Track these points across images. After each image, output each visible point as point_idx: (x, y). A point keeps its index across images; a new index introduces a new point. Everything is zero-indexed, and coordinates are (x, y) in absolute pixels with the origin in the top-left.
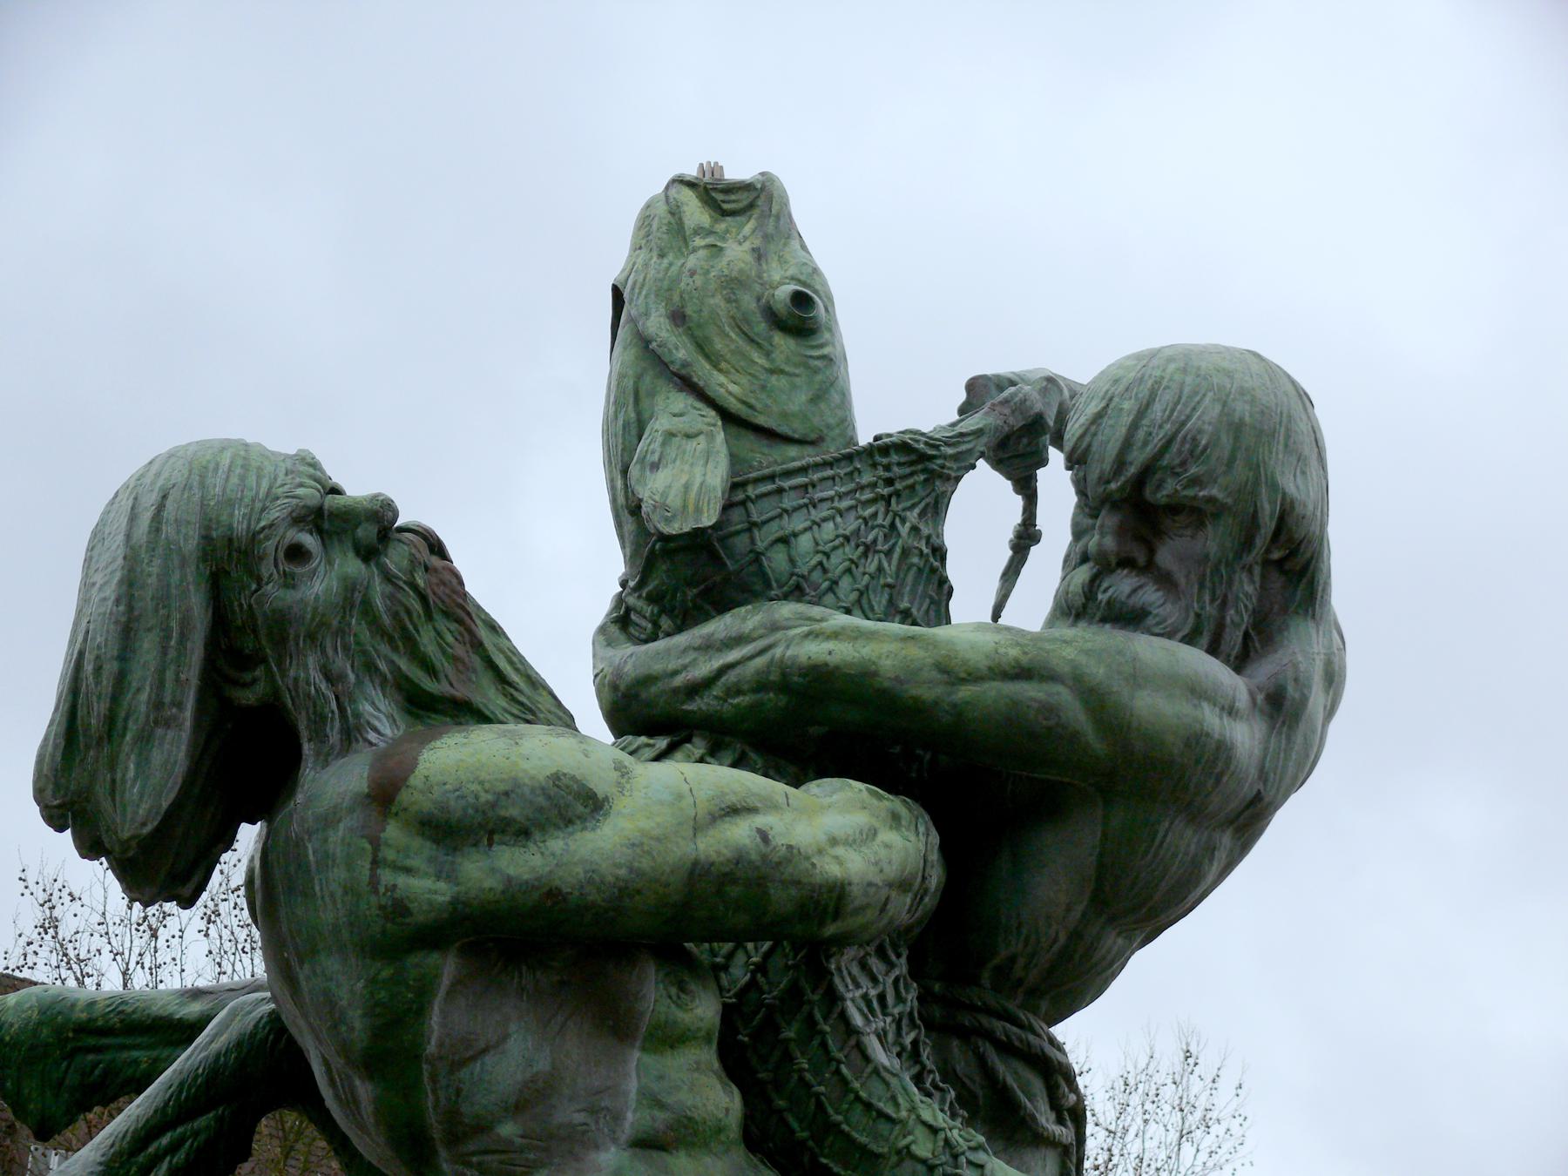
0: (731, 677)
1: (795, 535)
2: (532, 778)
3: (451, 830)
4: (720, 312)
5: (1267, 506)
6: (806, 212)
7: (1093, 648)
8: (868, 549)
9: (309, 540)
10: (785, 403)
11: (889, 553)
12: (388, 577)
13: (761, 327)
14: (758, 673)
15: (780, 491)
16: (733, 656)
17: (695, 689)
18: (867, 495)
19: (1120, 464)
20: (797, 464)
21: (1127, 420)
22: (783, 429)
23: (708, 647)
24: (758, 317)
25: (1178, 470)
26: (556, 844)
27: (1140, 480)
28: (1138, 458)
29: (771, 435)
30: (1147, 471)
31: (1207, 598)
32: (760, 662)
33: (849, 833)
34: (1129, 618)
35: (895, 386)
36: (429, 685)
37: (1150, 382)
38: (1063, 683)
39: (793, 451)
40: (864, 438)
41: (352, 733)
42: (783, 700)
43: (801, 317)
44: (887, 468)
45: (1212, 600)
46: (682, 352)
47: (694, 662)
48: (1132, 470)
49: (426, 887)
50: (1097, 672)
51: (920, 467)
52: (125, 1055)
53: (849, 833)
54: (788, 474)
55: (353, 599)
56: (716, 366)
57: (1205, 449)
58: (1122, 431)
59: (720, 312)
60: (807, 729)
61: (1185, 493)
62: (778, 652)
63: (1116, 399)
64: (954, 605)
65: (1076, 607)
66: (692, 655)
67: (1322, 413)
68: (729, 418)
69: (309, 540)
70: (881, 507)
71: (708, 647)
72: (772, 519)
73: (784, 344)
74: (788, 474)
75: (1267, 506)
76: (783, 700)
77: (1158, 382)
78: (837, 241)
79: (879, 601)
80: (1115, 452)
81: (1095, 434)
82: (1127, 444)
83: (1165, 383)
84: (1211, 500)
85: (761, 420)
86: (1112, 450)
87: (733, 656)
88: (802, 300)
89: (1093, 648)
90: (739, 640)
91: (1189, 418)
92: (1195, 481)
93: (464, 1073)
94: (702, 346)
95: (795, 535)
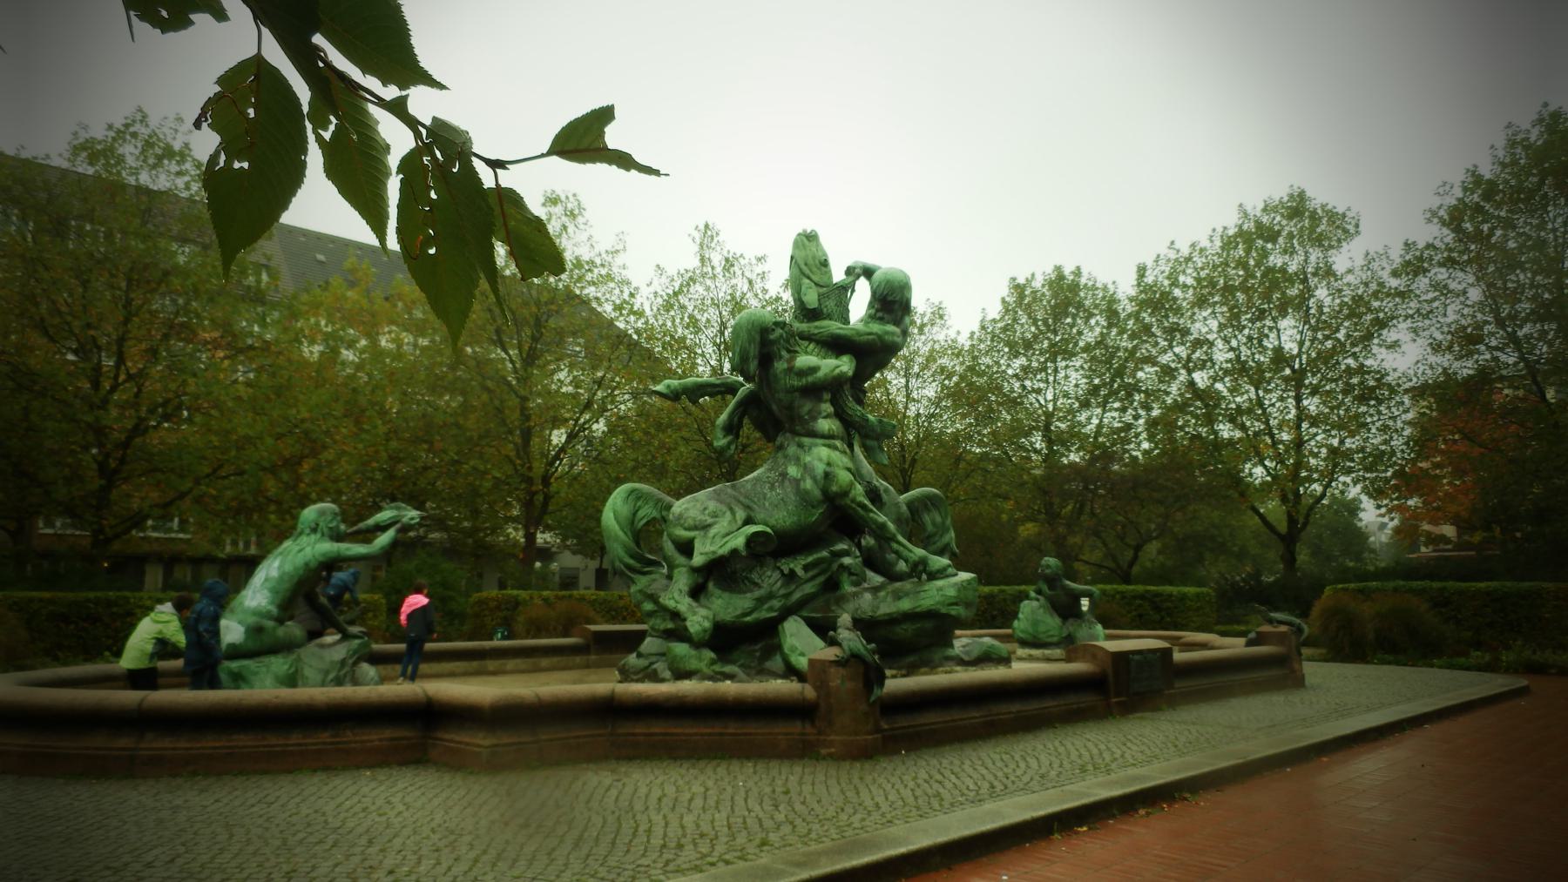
3: (803, 373)
4: (808, 259)
6: (823, 240)
7: (876, 328)
33: (845, 365)
35: (838, 275)
41: (781, 357)
43: (825, 264)
46: (807, 271)
49: (796, 383)
53: (845, 365)
59: (808, 259)
60: (837, 345)
65: (872, 317)
68: (817, 284)
89: (876, 328)
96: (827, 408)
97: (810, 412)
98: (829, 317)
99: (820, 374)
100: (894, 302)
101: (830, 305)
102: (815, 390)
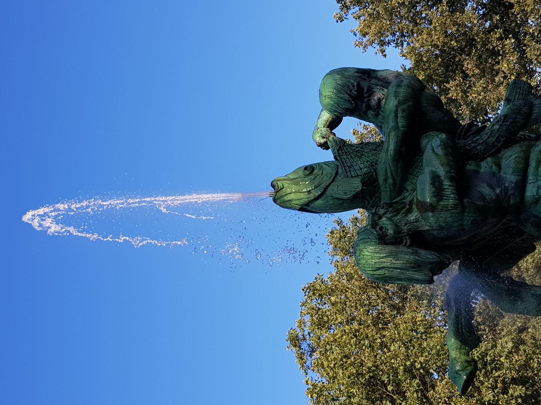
0: (395, 175)
8: (362, 155)
9: (378, 228)
10: (329, 171)
12: (385, 213)
13: (312, 177)
17: (394, 184)
18: (349, 157)
22: (336, 171)
26: (443, 178)
29: (337, 174)
30: (350, 95)
33: (434, 145)
36: (407, 207)
39: (340, 170)
42: (400, 161)
48: (350, 99)
49: (451, 200)
52: (463, 324)
53: (434, 145)
54: (345, 170)
55: (390, 219)
60: (408, 154)
69: (378, 228)
70: (352, 154)
73: (315, 172)
74: (345, 170)
76: (400, 161)
88: (306, 168)
92: (354, 86)
93: (487, 197)
96: (487, 165)
97: (491, 186)
98: (373, 165)
99: (441, 172)
100: (360, 88)
101: (361, 166)
102: (463, 182)
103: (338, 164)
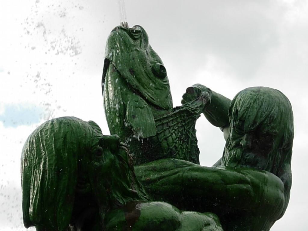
1: (168, 137)
2: (168, 218)
4: (131, 65)
5: (287, 135)
11: (188, 143)
14: (174, 179)
15: (163, 124)
16: (163, 174)
19: (255, 122)
20: (165, 116)
21: (256, 110)
22: (160, 106)
23: (154, 170)
24: (151, 72)
25: (269, 125)
27: (258, 128)
28: (259, 121)
30: (262, 123)
31: (271, 159)
32: (173, 177)
34: (253, 164)
37: (261, 100)
38: (250, 184)
39: (163, 112)
40: (174, 106)
44: (184, 117)
45: (272, 159)
46: (135, 83)
47: (149, 174)
50: (257, 181)
51: (190, 117)
56: (143, 87)
57: (276, 119)
58: (255, 113)
61: (270, 131)
62: (181, 174)
63: (252, 104)
64: (200, 157)
66: (148, 172)
67: (202, 84)
71: (154, 170)
72: (162, 132)
74: (164, 119)
75: (287, 135)
77: (263, 100)
78: (164, 47)
79: (188, 156)
80: (253, 119)
81: (247, 113)
82: (256, 117)
83: (265, 100)
84: (275, 133)
85: (156, 103)
86: (252, 118)
87: (163, 174)
90: (165, 169)
91: (272, 110)
92: (273, 128)
94: (139, 80)
95: (168, 137)
98: (171, 154)
101: (172, 136)
103: (170, 111)
